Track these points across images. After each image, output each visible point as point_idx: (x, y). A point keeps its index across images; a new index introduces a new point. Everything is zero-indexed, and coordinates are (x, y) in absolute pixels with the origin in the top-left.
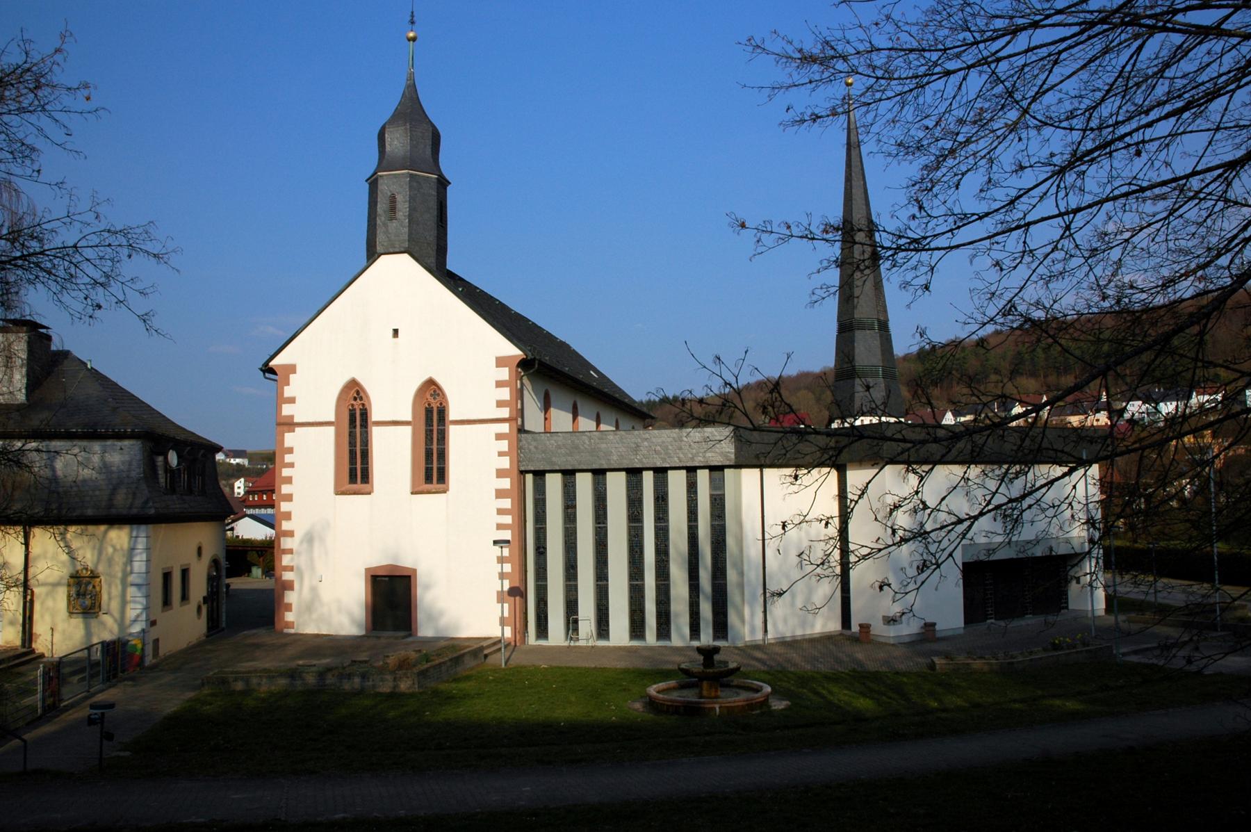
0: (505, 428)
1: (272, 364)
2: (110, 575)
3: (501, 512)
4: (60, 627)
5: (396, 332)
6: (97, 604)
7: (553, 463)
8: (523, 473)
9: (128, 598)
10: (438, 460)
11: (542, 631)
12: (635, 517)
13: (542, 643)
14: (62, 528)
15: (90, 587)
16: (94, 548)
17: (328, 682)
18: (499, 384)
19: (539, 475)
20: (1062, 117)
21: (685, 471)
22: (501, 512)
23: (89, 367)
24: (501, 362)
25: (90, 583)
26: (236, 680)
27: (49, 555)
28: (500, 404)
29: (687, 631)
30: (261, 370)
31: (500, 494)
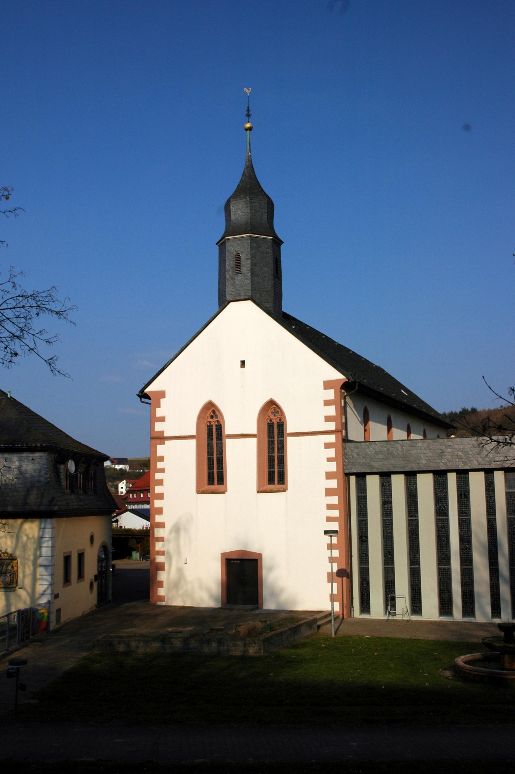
1: (147, 390)
2: (24, 558)
3: (330, 507)
5: (243, 363)
6: (15, 581)
8: (347, 475)
9: (38, 576)
11: (365, 606)
13: (365, 616)
15: (10, 567)
18: (327, 403)
19: (361, 476)
21: (483, 473)
22: (330, 507)
23: (9, 396)
24: (328, 385)
25: (10, 564)
26: (119, 643)
28: (328, 419)
30: (138, 395)
31: (329, 492)
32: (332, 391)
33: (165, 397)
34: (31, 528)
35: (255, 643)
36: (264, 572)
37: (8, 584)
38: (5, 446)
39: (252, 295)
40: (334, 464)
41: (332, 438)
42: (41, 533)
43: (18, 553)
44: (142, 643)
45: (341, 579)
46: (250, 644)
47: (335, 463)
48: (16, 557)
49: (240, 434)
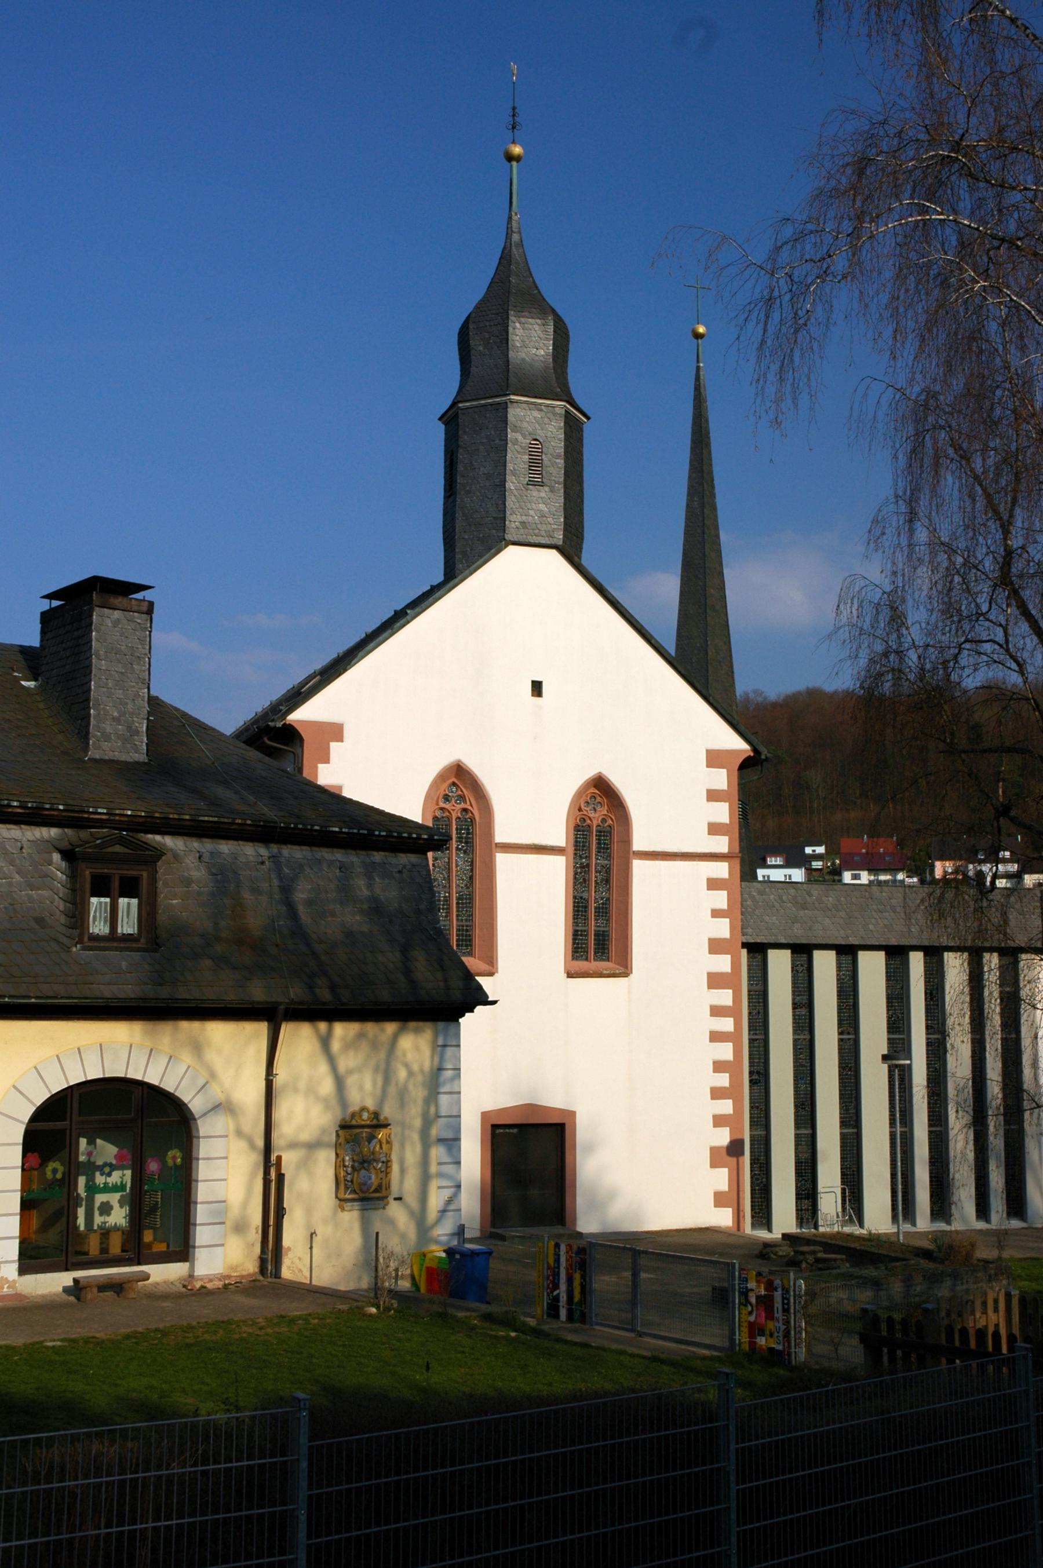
0: (721, 870)
1: (301, 715)
2: (403, 1125)
3: (717, 1011)
4: (324, 1232)
5: (537, 688)
8: (757, 950)
9: (433, 1169)
14: (323, 1026)
16: (376, 1070)
18: (713, 796)
19: (847, 953)
21: (789, 952)
22: (717, 1011)
24: (714, 758)
27: (302, 1085)
28: (714, 829)
31: (715, 981)
32: (723, 772)
33: (341, 740)
34: (417, 1049)
37: (371, 1190)
38: (351, 831)
42: (436, 1059)
43: (388, 1112)
47: (727, 920)
48: (386, 1118)
49: (530, 845)
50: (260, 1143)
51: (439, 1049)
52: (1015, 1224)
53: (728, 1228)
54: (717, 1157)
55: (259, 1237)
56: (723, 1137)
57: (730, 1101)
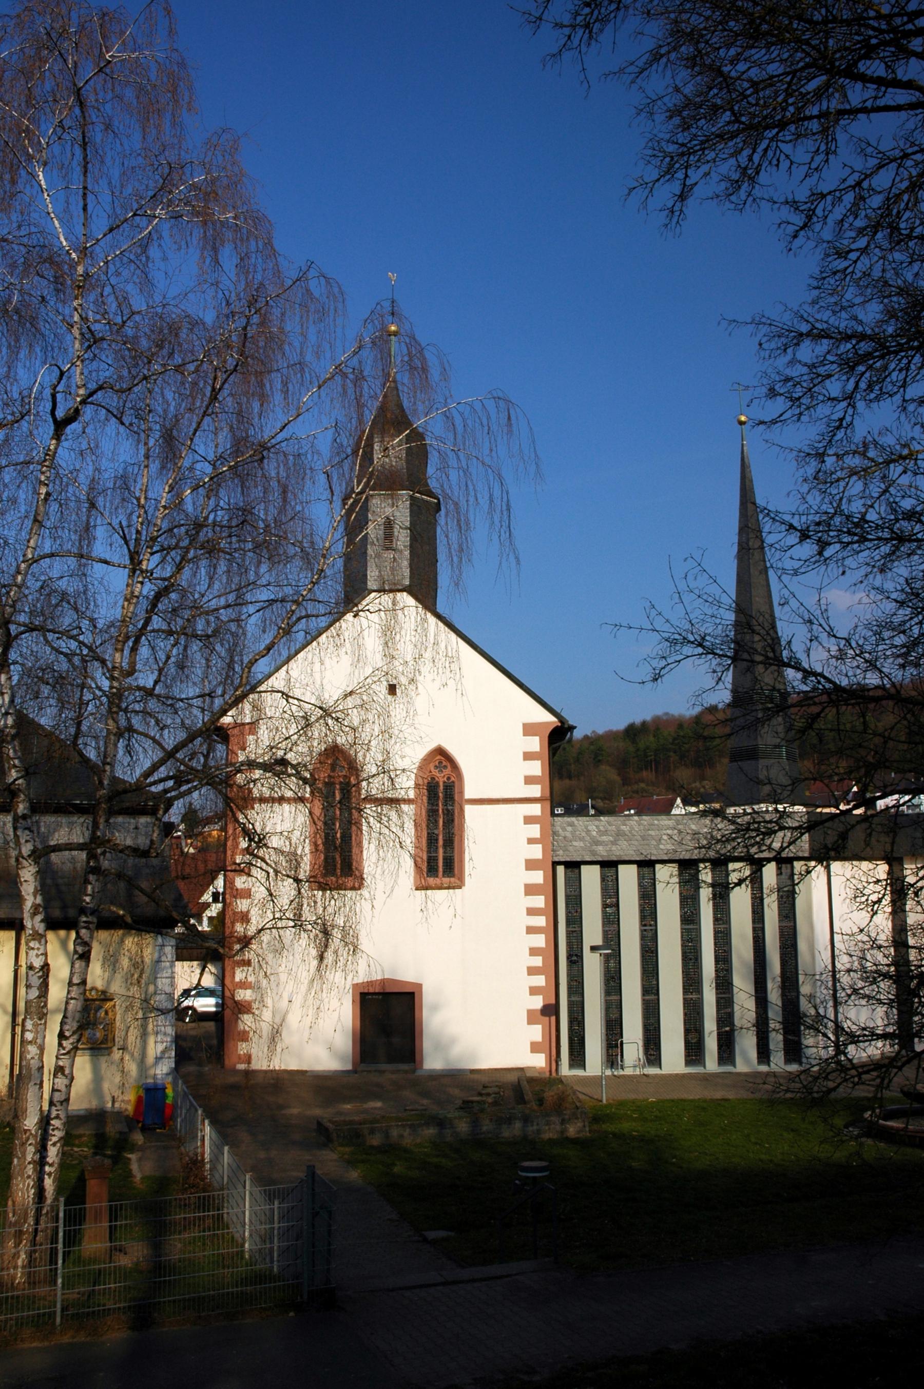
0: (536, 809)
3: (531, 912)
6: (110, 1037)
7: (593, 853)
8: (555, 864)
10: (445, 846)
11: (578, 1056)
12: (690, 919)
13: (579, 1072)
15: (102, 1014)
17: (485, 1128)
18: (528, 756)
19: (573, 866)
20: (315, 441)
21: (598, 867)
22: (531, 912)
24: (529, 729)
25: (101, 1007)
26: (372, 1131)
28: (529, 780)
29: (753, 1054)
31: (530, 890)
32: (537, 739)
35: (577, 1118)
36: (425, 1013)
39: (410, 586)
40: (539, 847)
41: (536, 809)
44: (408, 1130)
45: (547, 1018)
46: (570, 1119)
47: (540, 846)
50: (10, 1009)
51: (157, 948)
52: (794, 1068)
53: (542, 1068)
54: (532, 1017)
55: (8, 1072)
56: (538, 1003)
57: (543, 977)
